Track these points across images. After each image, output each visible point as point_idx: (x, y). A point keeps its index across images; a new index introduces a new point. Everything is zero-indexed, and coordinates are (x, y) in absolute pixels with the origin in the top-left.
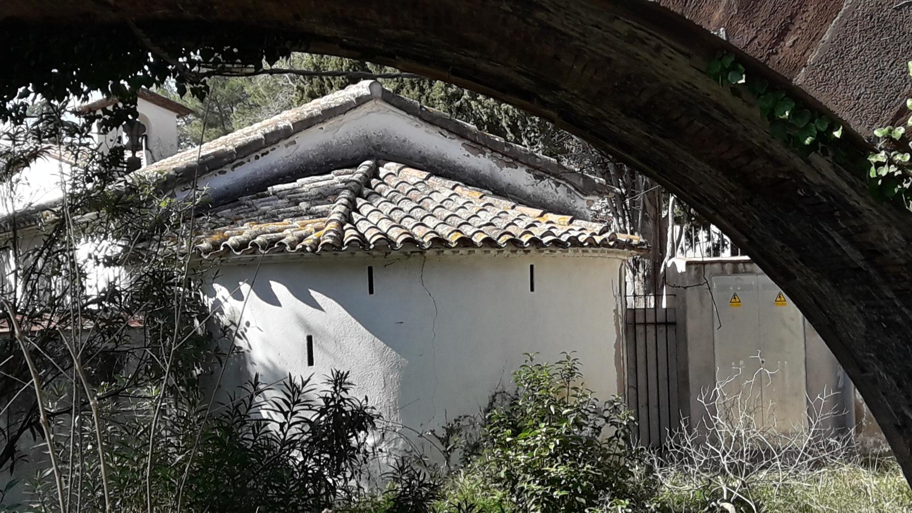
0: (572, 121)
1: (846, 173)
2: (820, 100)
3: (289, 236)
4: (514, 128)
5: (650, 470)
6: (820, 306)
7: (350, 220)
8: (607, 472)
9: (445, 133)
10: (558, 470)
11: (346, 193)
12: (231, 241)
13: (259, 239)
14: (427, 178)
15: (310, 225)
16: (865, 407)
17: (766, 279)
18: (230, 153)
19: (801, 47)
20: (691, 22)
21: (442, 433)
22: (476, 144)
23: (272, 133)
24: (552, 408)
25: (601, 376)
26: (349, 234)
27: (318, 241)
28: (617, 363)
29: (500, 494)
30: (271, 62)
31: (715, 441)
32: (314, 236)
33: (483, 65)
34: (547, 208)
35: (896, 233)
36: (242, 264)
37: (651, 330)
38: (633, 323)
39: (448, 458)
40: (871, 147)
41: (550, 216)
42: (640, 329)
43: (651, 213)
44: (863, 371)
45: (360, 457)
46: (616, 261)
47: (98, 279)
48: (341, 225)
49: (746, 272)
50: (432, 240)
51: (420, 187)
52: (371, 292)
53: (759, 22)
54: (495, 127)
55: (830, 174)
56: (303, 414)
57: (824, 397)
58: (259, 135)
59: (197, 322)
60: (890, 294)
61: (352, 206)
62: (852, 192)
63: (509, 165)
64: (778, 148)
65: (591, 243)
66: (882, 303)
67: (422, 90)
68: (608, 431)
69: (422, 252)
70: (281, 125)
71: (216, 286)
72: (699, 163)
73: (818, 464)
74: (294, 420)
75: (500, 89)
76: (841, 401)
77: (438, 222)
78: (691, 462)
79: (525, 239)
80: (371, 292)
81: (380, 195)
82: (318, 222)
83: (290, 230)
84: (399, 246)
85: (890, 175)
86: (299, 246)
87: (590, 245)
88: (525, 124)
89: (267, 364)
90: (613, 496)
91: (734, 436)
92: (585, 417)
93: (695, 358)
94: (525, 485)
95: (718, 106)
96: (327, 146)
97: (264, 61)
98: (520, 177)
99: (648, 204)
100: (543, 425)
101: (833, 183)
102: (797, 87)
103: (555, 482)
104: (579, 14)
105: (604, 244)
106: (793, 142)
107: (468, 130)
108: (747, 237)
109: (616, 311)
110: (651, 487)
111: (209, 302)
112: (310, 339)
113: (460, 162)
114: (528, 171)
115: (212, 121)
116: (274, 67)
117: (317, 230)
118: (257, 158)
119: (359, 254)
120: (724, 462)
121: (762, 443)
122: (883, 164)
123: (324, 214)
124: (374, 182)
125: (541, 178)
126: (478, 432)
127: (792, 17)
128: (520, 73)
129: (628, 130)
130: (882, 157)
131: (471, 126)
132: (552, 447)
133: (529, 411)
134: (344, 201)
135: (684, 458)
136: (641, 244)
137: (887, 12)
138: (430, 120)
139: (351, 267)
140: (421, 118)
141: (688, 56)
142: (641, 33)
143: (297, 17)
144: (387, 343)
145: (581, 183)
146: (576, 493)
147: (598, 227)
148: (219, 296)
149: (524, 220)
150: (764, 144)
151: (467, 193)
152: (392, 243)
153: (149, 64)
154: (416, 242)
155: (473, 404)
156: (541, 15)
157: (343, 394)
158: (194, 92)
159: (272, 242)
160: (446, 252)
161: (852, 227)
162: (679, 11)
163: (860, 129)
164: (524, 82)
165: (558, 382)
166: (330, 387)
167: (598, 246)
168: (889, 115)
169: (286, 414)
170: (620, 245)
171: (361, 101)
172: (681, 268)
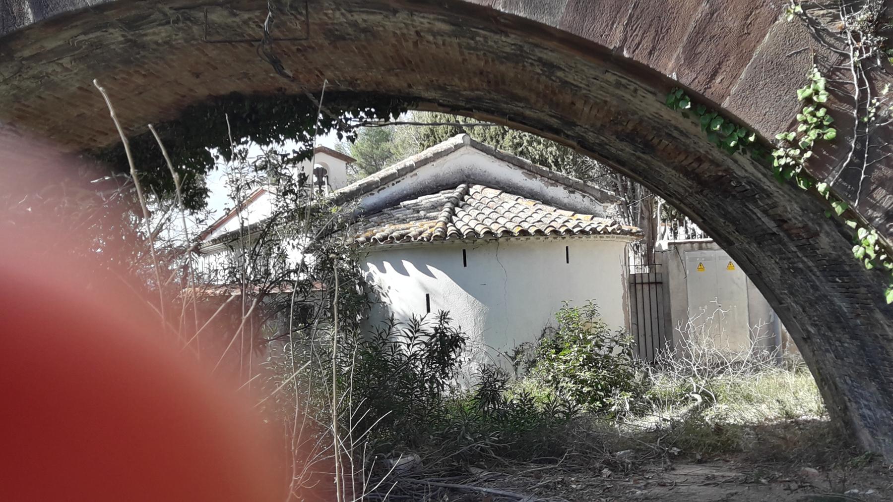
0: (586, 147)
1: (760, 167)
2: (740, 117)
3: (413, 232)
4: (556, 163)
5: (646, 375)
6: (751, 262)
7: (451, 221)
8: (617, 376)
9: (511, 165)
10: (586, 375)
11: (449, 205)
12: (378, 236)
13: (394, 234)
14: (500, 194)
15: (426, 224)
16: (788, 334)
17: (723, 253)
18: (377, 182)
19: (726, 83)
20: (654, 69)
21: (512, 354)
22: (532, 172)
23: (402, 169)
24: (581, 335)
25: (614, 316)
26: (451, 230)
27: (431, 234)
28: (624, 309)
29: (548, 390)
30: (396, 116)
31: (688, 356)
32: (429, 231)
33: (528, 112)
34: (576, 211)
35: (795, 206)
36: (384, 250)
37: (646, 287)
38: (634, 283)
39: (516, 370)
40: (773, 147)
41: (578, 216)
42: (639, 287)
43: (646, 214)
44: (781, 303)
45: (457, 364)
46: (621, 244)
47: (294, 257)
48: (446, 224)
49: (708, 249)
50: (503, 232)
51: (495, 200)
52: (465, 265)
53: (698, 68)
54: (544, 162)
55: (751, 169)
56: (421, 338)
57: (761, 325)
58: (395, 171)
59: (358, 287)
60: (794, 249)
61: (453, 213)
62: (764, 180)
63: (552, 185)
64: (716, 154)
65: (606, 232)
66: (790, 255)
67: (498, 141)
68: (617, 350)
69: (497, 239)
70: (408, 164)
71: (369, 264)
72: (669, 170)
73: (757, 370)
74: (416, 342)
75: (538, 128)
76: (772, 328)
77: (506, 220)
78: (673, 369)
79: (562, 230)
80: (465, 265)
81: (470, 205)
82: (432, 223)
83: (413, 228)
84: (482, 236)
85: (787, 165)
86: (419, 238)
87: (605, 233)
88: (563, 160)
89: (401, 312)
90: (621, 390)
91: (701, 352)
92: (602, 341)
93: (675, 304)
94: (564, 384)
95: (676, 128)
96: (437, 176)
97: (391, 115)
98: (559, 192)
99: (644, 208)
100: (575, 346)
101: (753, 175)
102: (724, 110)
103: (583, 382)
104: (583, 71)
105: (613, 232)
106: (722, 144)
107: (525, 163)
108: (703, 218)
109: (623, 275)
110: (647, 384)
111: (365, 275)
112: (428, 296)
113: (520, 184)
114: (565, 189)
115: (371, 170)
116: (398, 120)
117: (430, 227)
118: (393, 184)
119: (457, 241)
120: (695, 369)
121: (720, 358)
122: (782, 157)
123: (435, 218)
124: (466, 197)
125: (573, 192)
126: (534, 354)
127: (720, 64)
128: (551, 116)
129: (622, 150)
130: (781, 152)
131: (529, 161)
132: (581, 359)
133: (566, 337)
134: (448, 209)
135: (668, 366)
136: (638, 232)
137: (783, 58)
138: (502, 158)
139: (454, 250)
140: (495, 157)
141: (654, 94)
142: (624, 81)
143: (410, 86)
144: (477, 298)
145: (599, 195)
146: (598, 389)
147: (609, 222)
148: (371, 271)
149: (561, 219)
150: (707, 152)
151: (525, 203)
152: (477, 234)
153: (320, 121)
154: (493, 233)
155: (530, 334)
156: (560, 74)
157: (446, 325)
158: (348, 138)
159: (402, 236)
160: (512, 239)
161: (767, 205)
162: (646, 63)
163: (766, 134)
164: (554, 122)
165: (584, 319)
166: (437, 321)
167: (610, 233)
168: (785, 125)
169: (411, 338)
170: (624, 233)
171: (457, 147)
172: (665, 247)
